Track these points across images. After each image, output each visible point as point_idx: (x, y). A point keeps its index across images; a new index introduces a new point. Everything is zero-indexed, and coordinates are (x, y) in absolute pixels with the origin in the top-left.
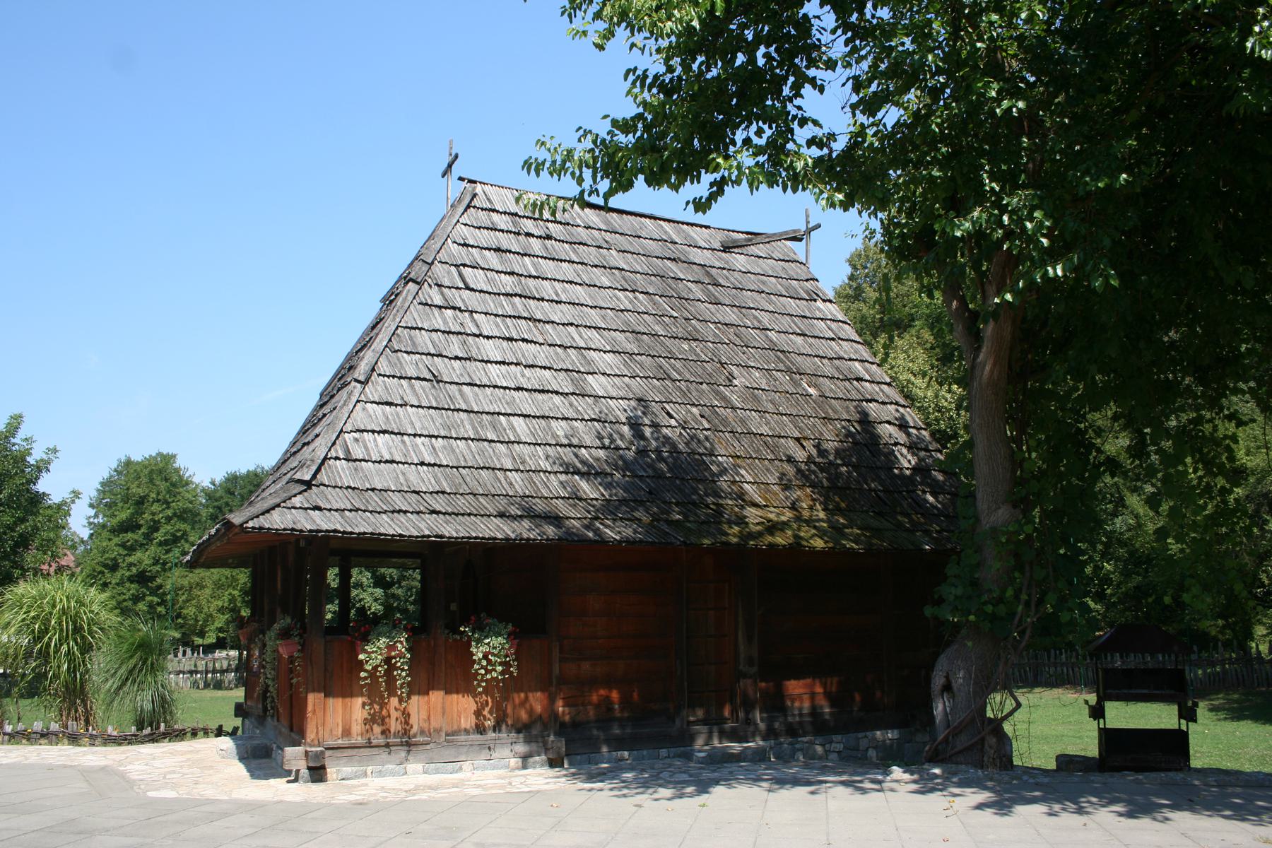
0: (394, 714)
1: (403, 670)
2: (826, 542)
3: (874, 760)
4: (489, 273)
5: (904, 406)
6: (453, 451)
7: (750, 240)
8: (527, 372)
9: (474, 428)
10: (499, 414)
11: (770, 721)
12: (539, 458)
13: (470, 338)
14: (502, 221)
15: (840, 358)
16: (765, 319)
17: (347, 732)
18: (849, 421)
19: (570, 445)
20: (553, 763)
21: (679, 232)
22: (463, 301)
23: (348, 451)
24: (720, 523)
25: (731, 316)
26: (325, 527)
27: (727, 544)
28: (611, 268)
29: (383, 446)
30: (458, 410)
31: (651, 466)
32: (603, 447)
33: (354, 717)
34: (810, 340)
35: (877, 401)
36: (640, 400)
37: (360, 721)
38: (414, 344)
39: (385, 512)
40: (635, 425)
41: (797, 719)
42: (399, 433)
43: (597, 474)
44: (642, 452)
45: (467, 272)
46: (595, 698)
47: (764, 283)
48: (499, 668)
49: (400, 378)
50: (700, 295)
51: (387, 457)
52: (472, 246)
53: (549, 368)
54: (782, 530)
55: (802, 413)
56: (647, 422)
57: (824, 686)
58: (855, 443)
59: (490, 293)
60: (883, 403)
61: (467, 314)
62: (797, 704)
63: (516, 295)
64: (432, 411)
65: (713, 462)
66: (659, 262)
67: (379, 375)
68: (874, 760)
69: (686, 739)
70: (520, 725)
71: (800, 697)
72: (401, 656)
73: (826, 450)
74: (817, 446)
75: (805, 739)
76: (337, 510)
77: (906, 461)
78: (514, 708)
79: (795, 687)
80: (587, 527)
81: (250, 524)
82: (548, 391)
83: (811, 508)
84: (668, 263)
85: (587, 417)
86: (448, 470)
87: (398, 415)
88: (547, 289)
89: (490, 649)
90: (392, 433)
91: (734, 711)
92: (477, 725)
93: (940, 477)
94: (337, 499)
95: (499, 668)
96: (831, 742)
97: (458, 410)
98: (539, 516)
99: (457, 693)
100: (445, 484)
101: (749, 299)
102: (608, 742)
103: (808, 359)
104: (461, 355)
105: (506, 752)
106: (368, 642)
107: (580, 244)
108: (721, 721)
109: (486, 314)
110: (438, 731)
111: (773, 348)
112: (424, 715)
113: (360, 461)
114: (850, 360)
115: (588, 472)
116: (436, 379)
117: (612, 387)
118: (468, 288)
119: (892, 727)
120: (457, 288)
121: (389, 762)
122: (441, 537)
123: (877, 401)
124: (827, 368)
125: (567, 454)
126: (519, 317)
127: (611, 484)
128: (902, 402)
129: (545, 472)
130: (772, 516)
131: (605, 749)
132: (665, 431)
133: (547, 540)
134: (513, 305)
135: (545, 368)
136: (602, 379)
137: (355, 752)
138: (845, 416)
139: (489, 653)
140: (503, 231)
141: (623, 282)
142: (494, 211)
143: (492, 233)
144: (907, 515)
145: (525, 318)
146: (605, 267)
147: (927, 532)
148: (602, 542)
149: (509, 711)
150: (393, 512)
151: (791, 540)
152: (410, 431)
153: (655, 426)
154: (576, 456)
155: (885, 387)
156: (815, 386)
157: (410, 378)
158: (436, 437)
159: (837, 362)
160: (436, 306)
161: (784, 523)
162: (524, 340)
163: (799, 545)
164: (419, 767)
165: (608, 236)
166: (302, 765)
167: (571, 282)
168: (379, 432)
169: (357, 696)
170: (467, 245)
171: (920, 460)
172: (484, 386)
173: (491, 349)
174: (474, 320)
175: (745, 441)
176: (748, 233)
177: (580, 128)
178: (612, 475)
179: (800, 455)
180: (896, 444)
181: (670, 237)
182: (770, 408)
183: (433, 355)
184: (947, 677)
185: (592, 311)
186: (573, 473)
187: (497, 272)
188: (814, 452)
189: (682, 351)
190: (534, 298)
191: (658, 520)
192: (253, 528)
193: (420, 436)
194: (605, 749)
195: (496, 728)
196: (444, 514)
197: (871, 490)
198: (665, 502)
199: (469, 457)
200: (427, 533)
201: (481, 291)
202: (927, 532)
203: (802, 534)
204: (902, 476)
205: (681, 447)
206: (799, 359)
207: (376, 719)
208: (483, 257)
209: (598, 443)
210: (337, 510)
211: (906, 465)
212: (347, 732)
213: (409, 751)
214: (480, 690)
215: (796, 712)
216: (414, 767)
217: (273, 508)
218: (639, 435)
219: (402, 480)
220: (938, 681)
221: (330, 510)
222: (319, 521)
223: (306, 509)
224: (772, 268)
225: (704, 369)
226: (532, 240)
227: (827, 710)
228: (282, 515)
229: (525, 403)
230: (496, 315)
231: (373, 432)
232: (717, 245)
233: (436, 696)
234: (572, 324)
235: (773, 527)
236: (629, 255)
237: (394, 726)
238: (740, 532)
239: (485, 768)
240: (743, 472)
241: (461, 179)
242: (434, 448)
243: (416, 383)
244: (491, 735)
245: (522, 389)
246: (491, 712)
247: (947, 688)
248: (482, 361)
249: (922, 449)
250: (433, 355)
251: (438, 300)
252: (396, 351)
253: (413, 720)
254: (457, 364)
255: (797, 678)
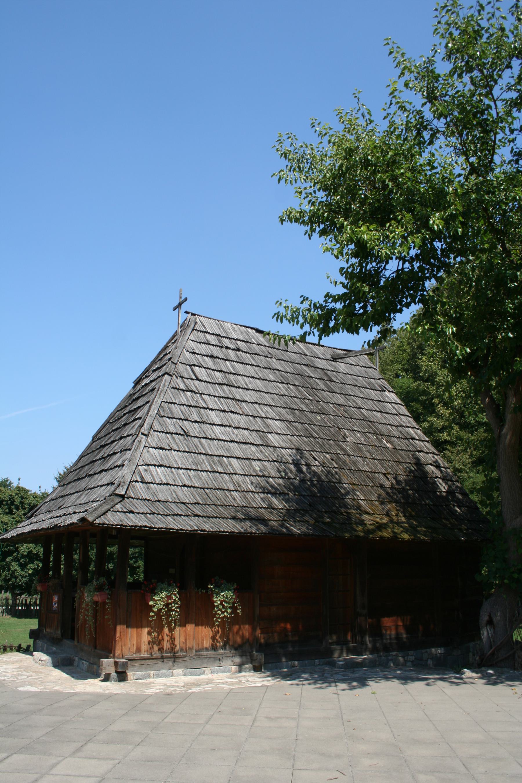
0: (166, 638)
1: (176, 611)
2: (410, 536)
3: (431, 666)
4: (208, 370)
5: (437, 455)
6: (200, 478)
7: (346, 354)
8: (235, 431)
9: (210, 465)
10: (223, 456)
11: (374, 642)
12: (247, 484)
13: (202, 410)
14: (212, 339)
15: (402, 426)
16: (359, 401)
17: (138, 650)
18: (410, 463)
19: (264, 476)
20: (256, 669)
21: (308, 348)
22: (196, 387)
23: (142, 478)
24: (351, 524)
25: (341, 400)
26: (139, 524)
27: (358, 537)
28: (274, 370)
29: (160, 474)
30: (200, 453)
31: (308, 489)
32: (282, 478)
33: (143, 641)
34: (385, 415)
35: (423, 452)
36: (298, 449)
37: (146, 643)
38: (172, 413)
39: (169, 515)
40: (297, 464)
41: (389, 641)
42: (169, 467)
43: (280, 494)
44: (303, 481)
45: (196, 369)
46: (278, 629)
47: (356, 380)
48: (229, 610)
49: (167, 433)
50: (323, 387)
51: (164, 481)
52: (198, 354)
53: (247, 429)
54: (385, 528)
55: (385, 458)
56: (303, 463)
57: (403, 621)
58: (415, 476)
59: (210, 383)
60: (427, 453)
61: (198, 395)
62: (388, 632)
63: (224, 384)
64: (186, 454)
65: (341, 487)
66: (298, 366)
67: (155, 431)
68: (431, 666)
69: (329, 653)
70: (236, 645)
71: (390, 627)
72: (175, 602)
73: (400, 481)
74: (395, 478)
75: (394, 653)
76: (142, 514)
77: (443, 487)
78: (233, 635)
79: (387, 622)
80: (282, 526)
81: (97, 521)
82: (248, 443)
83: (397, 515)
84: (304, 367)
85: (271, 460)
86: (199, 489)
87: (167, 456)
88: (241, 381)
89: (223, 598)
90: (166, 466)
91: (354, 636)
92: (212, 645)
93: (460, 497)
94: (141, 507)
95: (229, 610)
96: (408, 655)
97: (200, 453)
98: (254, 519)
99: (202, 625)
100: (199, 498)
101: (350, 390)
102: (285, 655)
103: (384, 426)
104: (198, 420)
105: (229, 662)
106: (155, 594)
107: (256, 354)
108: (346, 643)
109: (209, 395)
110: (191, 649)
111: (365, 419)
112: (183, 640)
113: (150, 483)
114: (407, 427)
115: (276, 492)
116: (186, 434)
117: (282, 440)
118: (198, 379)
119: (440, 646)
120: (192, 379)
121: (163, 669)
122: (204, 531)
123: (423, 452)
124: (396, 433)
125: (263, 483)
126: (228, 398)
127: (288, 499)
128: (436, 452)
129: (252, 492)
130: (378, 520)
131: (284, 660)
132: (313, 468)
133: (262, 533)
134: (224, 390)
135: (245, 429)
136: (276, 436)
137: (143, 662)
138: (408, 461)
139: (224, 601)
140: (213, 345)
141: (281, 378)
142: (207, 332)
143: (207, 346)
144: (448, 520)
145: (231, 399)
146: (270, 369)
147: (460, 530)
148: (291, 535)
149: (231, 637)
150: (173, 515)
151: (392, 535)
152: (175, 466)
153: (308, 465)
154: (268, 483)
155: (426, 443)
156: (390, 442)
157: (172, 433)
158: (190, 470)
159: (400, 428)
160: (182, 390)
161: (385, 524)
162: (232, 412)
163: (396, 537)
164: (180, 671)
165: (270, 350)
166: (112, 671)
167: (253, 377)
168: (158, 466)
169: (145, 627)
170: (195, 353)
171: (449, 487)
172: (213, 439)
173: (214, 417)
174: (203, 399)
175: (357, 475)
176: (344, 350)
177: (302, 296)
178: (288, 494)
179: (387, 484)
180: (437, 477)
181: (304, 352)
182: (368, 455)
183: (183, 420)
184: (490, 616)
185: (266, 395)
186: (267, 493)
187: (213, 370)
188: (394, 482)
189: (318, 421)
190: (234, 387)
191: (318, 522)
192: (99, 524)
193: (181, 468)
194: (284, 660)
195: (224, 647)
196: (202, 517)
197: (426, 504)
198: (319, 511)
199: (210, 482)
200: (196, 528)
201: (205, 382)
202: (460, 530)
203: (396, 531)
204: (441, 496)
205: (323, 477)
206: (380, 426)
207: (156, 642)
208: (204, 361)
209: (278, 475)
210: (142, 514)
211: (444, 490)
212: (138, 650)
213: (174, 661)
214: (217, 623)
215: (388, 637)
216: (177, 671)
217: (107, 512)
218: (300, 471)
219: (175, 496)
220: (484, 618)
221: (138, 513)
222: (134, 520)
223: (125, 512)
224: (360, 372)
225: (330, 431)
226: (230, 351)
227: (405, 636)
228: (113, 516)
229: (237, 450)
230: (215, 396)
231: (155, 465)
232: (329, 357)
233: (190, 628)
234: (256, 403)
235: (380, 527)
236: (282, 362)
237: (166, 645)
238: (363, 529)
239: (218, 672)
240: (358, 493)
241: (186, 312)
242: (189, 476)
243: (176, 436)
244: (221, 651)
245: (234, 441)
246: (220, 637)
247: (490, 622)
248: (210, 424)
249: (449, 480)
250: (183, 420)
251: (182, 386)
252: (162, 417)
253: (177, 642)
254: (196, 425)
255: (388, 616)
